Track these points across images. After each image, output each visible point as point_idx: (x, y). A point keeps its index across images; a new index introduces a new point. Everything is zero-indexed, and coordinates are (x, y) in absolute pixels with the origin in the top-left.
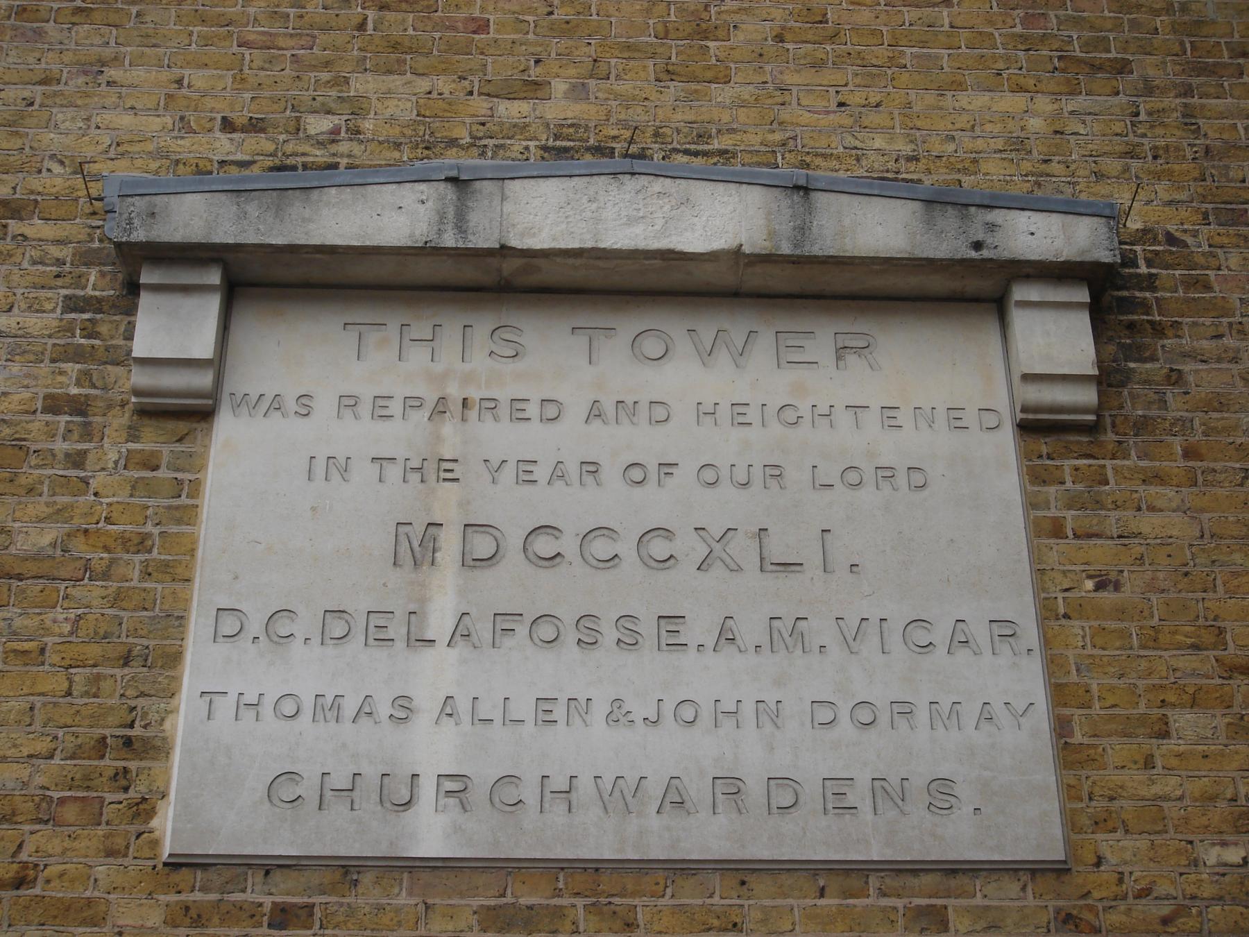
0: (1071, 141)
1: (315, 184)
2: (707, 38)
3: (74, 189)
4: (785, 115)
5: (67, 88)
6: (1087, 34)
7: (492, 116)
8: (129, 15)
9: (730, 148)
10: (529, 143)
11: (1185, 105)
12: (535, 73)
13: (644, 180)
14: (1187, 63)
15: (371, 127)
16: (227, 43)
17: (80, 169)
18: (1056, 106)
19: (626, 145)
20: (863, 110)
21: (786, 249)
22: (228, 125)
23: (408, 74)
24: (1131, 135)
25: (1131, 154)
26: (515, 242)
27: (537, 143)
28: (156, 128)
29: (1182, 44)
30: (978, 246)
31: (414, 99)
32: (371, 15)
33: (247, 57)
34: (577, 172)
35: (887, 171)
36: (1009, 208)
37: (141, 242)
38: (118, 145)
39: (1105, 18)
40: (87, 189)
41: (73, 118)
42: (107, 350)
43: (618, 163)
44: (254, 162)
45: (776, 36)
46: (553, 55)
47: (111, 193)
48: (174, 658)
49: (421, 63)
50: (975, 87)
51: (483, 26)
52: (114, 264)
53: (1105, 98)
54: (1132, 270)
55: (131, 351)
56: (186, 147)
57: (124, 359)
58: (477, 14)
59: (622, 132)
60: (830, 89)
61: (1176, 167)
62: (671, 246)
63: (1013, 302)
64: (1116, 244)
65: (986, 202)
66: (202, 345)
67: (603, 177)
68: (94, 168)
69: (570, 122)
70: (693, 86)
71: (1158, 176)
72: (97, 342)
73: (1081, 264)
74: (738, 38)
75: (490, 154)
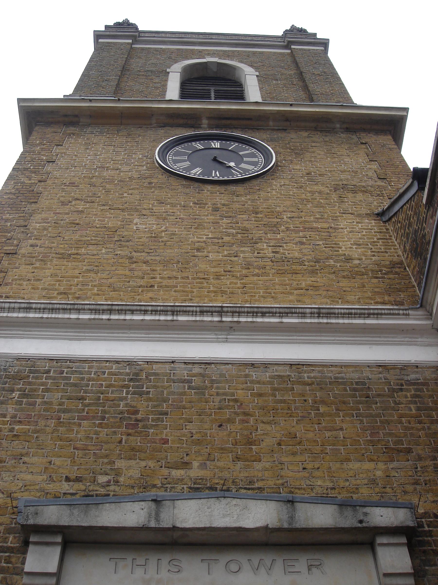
0: (393, 479)
1: (100, 502)
2: (252, 445)
3: (6, 503)
4: (283, 473)
5: (8, 464)
6: (394, 439)
7: (170, 476)
8: (33, 437)
9: (262, 487)
10: (184, 486)
11: (434, 464)
12: (186, 459)
13: (229, 500)
14: (433, 448)
15: (123, 480)
16: (69, 448)
17: (10, 496)
18: (386, 466)
19: (222, 486)
20: (313, 470)
21: (286, 526)
22: (68, 479)
23: (138, 460)
24: (415, 476)
25: (416, 483)
26: (179, 525)
27: (187, 486)
28: (40, 480)
29: (430, 441)
30: (361, 522)
31: (140, 469)
32: (124, 438)
33: (77, 453)
34: (203, 497)
35: (324, 494)
36: (371, 506)
37: (32, 524)
38: (25, 486)
39: (401, 433)
40: (12, 503)
41: (9, 476)
42: (14, 568)
43: (219, 493)
44: (77, 494)
45: (278, 444)
46: (193, 452)
47: (21, 505)
49: (143, 455)
50: (355, 460)
51: (166, 442)
52: (20, 533)
53: (404, 462)
54: (422, 529)
55: (24, 569)
56: (51, 487)
57: (20, 572)
58: (164, 437)
59: (220, 481)
60: (299, 463)
61: (434, 488)
62: (241, 526)
63: (377, 544)
64: (414, 518)
65: (363, 504)
66: (53, 567)
67: (213, 499)
68: (15, 495)
69: (199, 478)
70: (247, 463)
71: (428, 491)
72: (10, 565)
73: (402, 527)
74: (263, 445)
75: (169, 490)
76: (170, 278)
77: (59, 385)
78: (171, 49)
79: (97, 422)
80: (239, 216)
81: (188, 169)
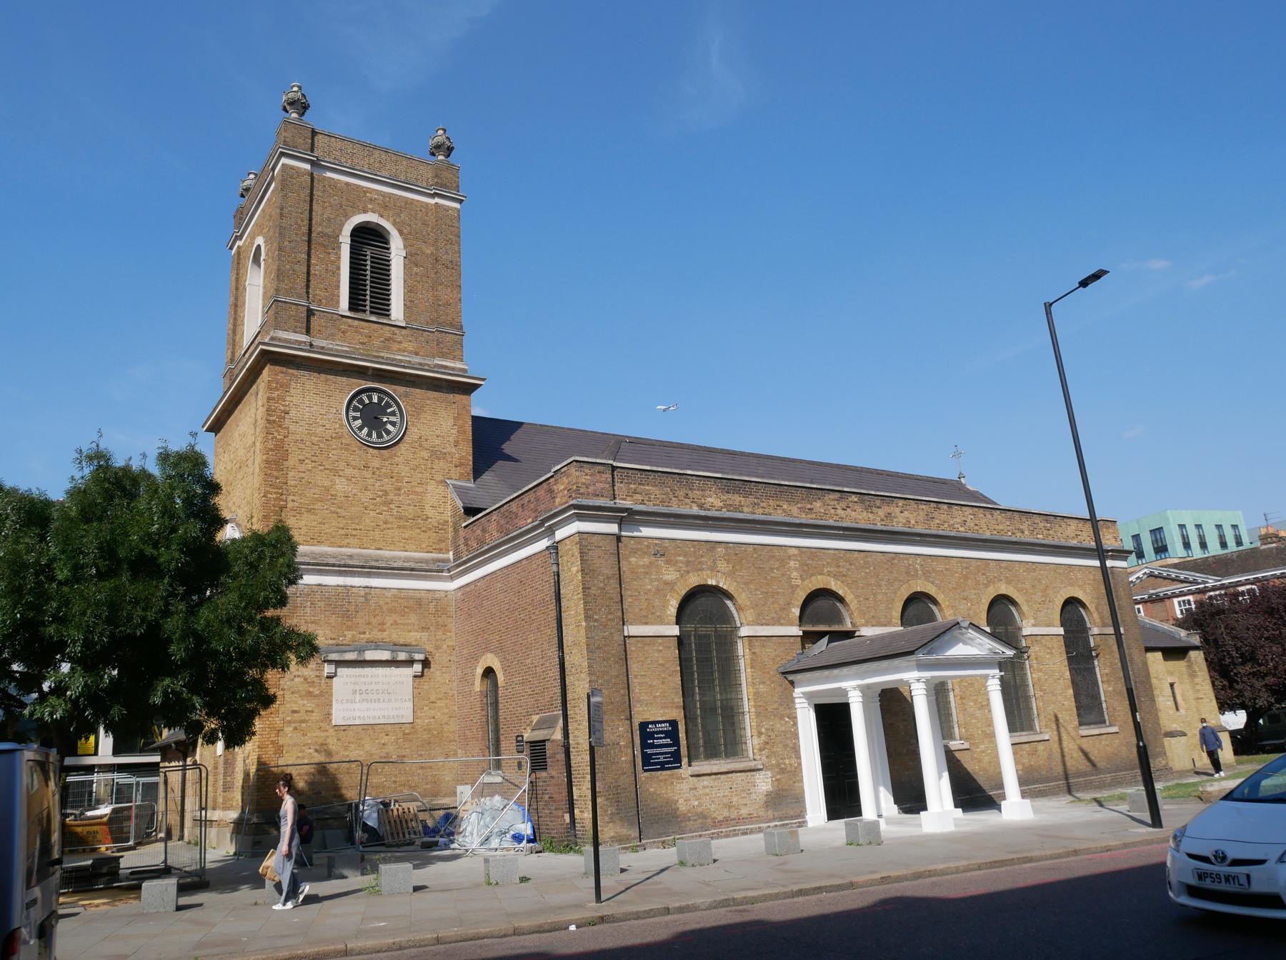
48: (332, 705)
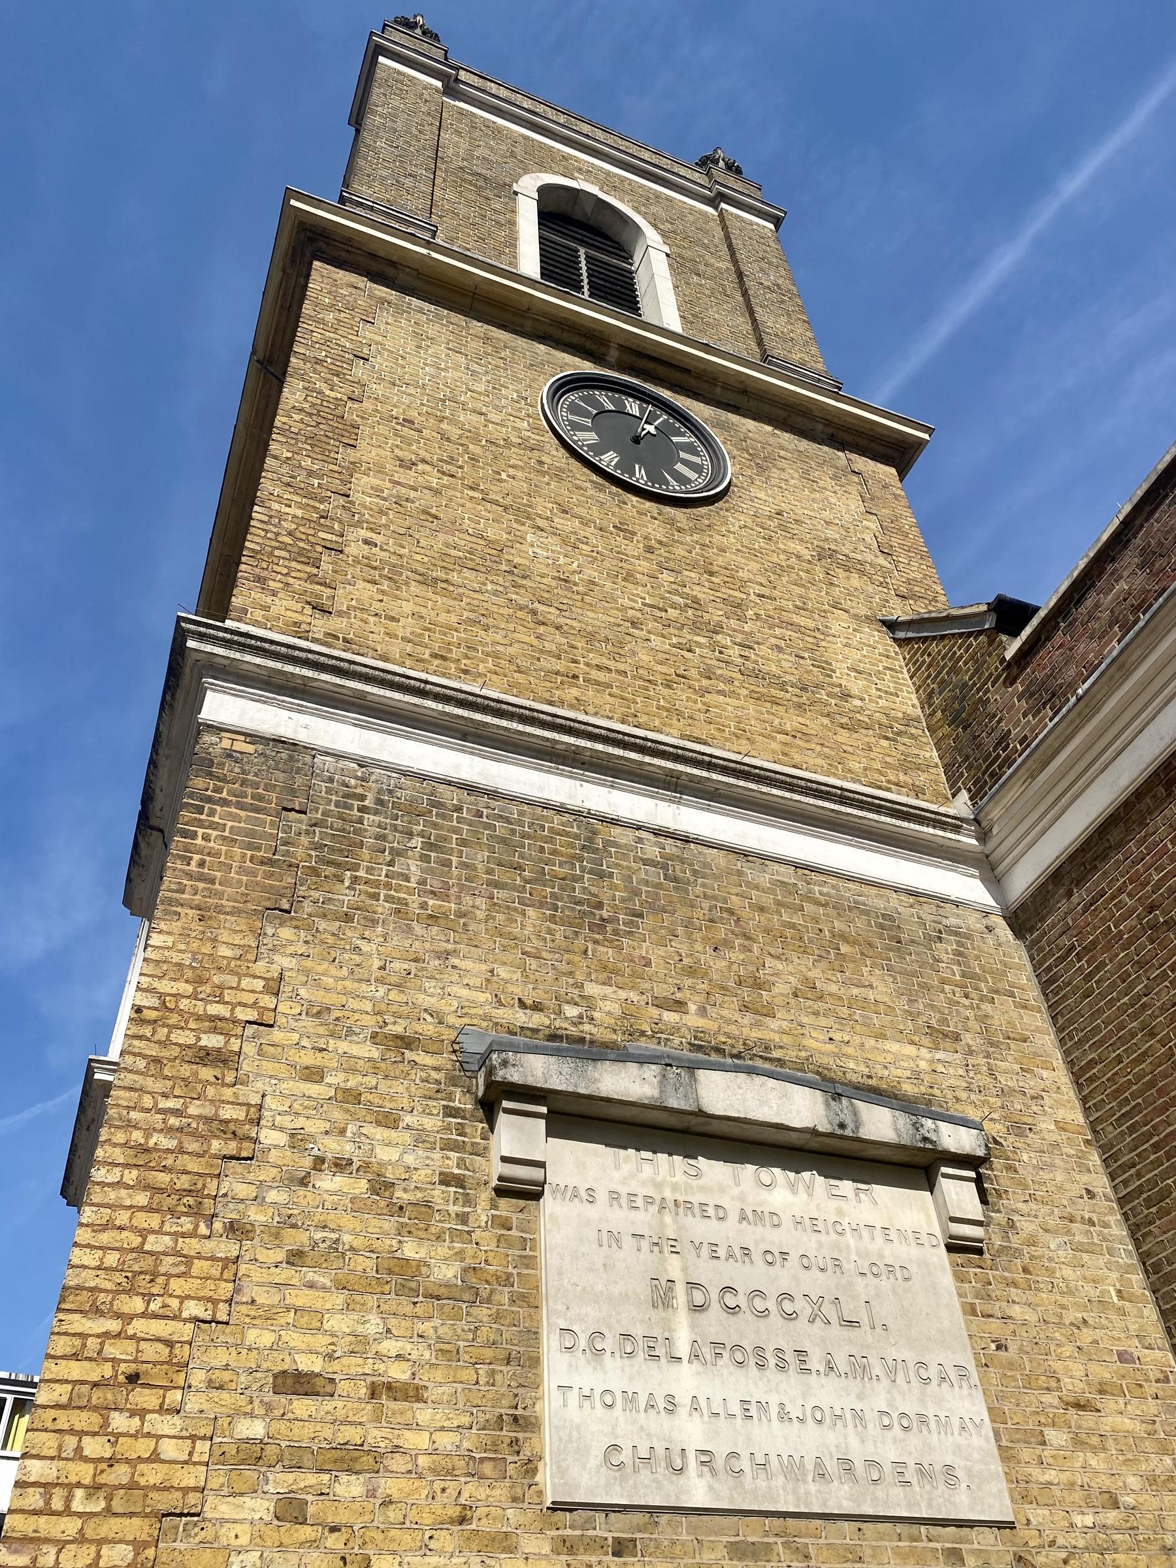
22: (522, 1004)
32: (590, 946)
70: (758, 1017)
76: (599, 667)
77: (480, 836)
78: (512, 131)
79: (548, 912)
80: (685, 573)
81: (599, 449)
